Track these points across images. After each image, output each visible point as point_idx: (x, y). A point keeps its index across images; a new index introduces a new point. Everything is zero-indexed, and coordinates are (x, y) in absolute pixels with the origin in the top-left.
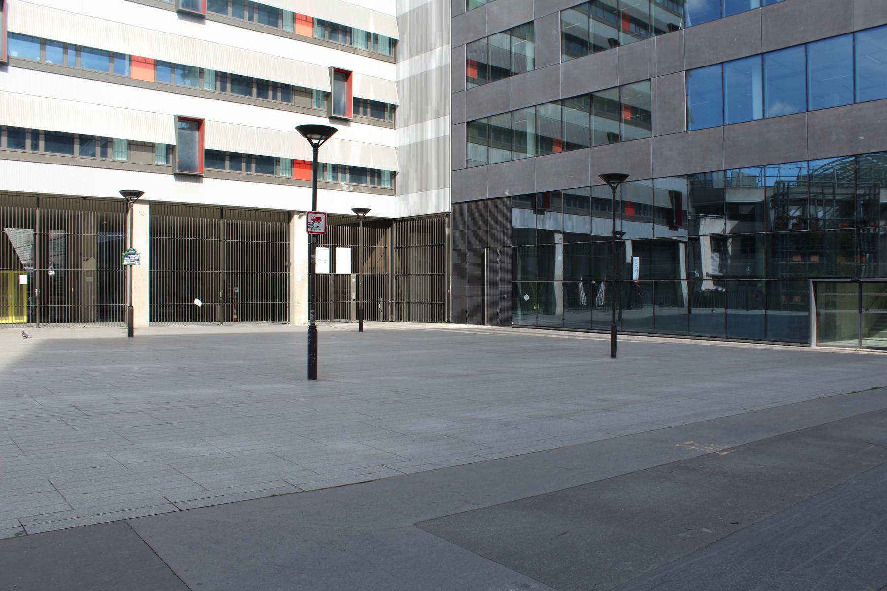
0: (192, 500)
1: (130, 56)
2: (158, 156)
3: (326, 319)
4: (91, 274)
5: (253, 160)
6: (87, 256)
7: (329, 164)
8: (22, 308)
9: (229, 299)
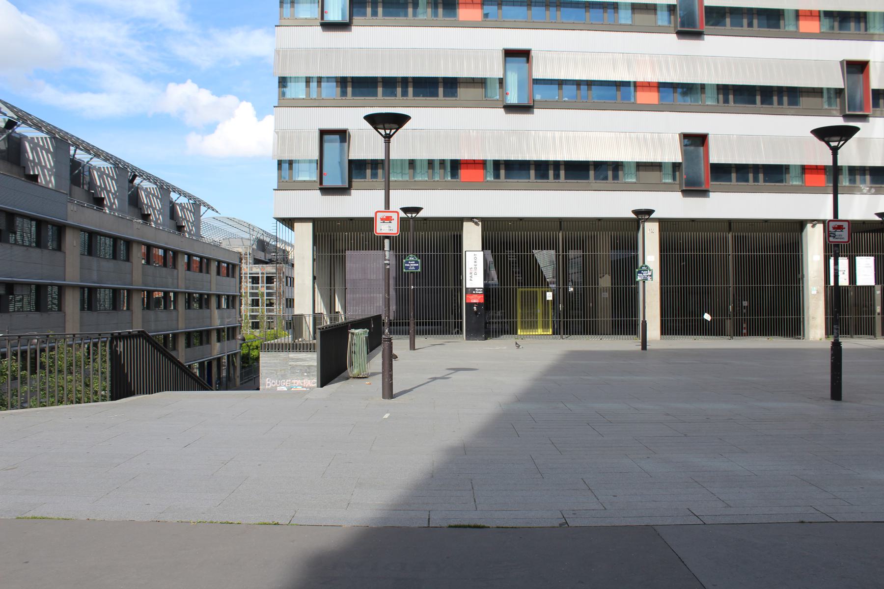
0: (716, 515)
1: (635, 82)
3: (846, 334)
4: (606, 290)
5: (761, 170)
6: (603, 273)
7: (845, 166)
8: (548, 321)
9: (739, 313)
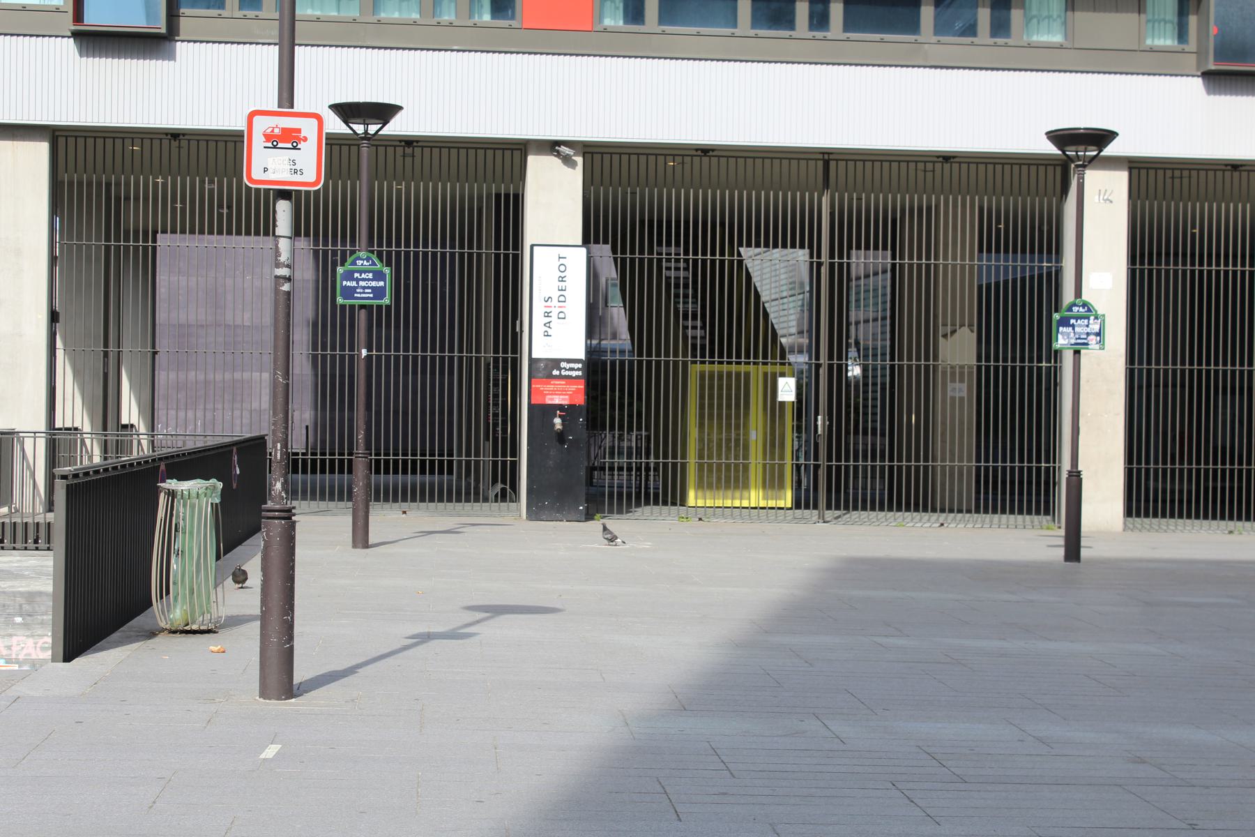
2: (1154, 21)
4: (962, 374)
6: (953, 324)
8: (782, 467)
